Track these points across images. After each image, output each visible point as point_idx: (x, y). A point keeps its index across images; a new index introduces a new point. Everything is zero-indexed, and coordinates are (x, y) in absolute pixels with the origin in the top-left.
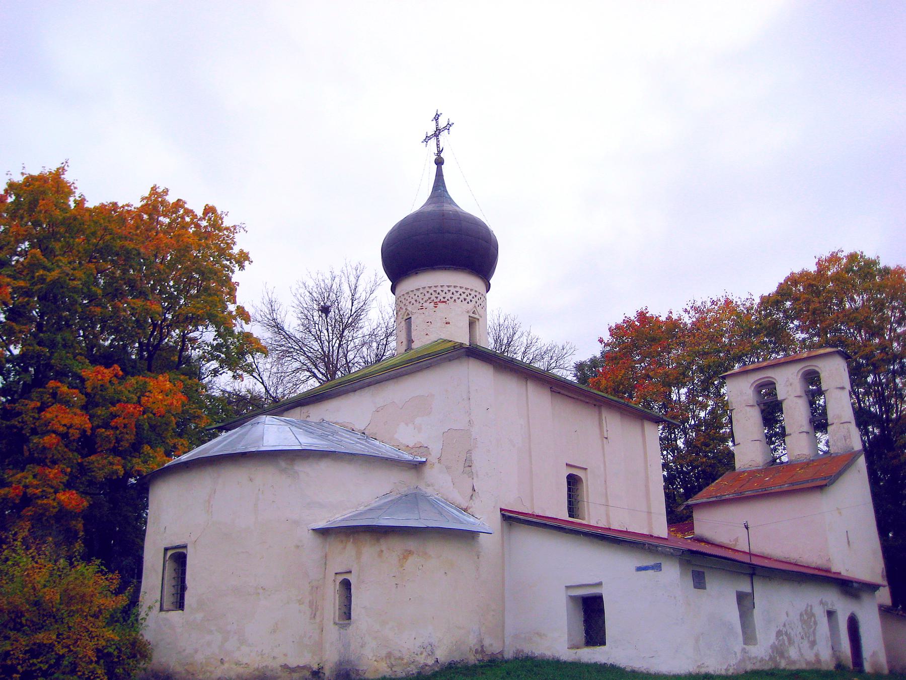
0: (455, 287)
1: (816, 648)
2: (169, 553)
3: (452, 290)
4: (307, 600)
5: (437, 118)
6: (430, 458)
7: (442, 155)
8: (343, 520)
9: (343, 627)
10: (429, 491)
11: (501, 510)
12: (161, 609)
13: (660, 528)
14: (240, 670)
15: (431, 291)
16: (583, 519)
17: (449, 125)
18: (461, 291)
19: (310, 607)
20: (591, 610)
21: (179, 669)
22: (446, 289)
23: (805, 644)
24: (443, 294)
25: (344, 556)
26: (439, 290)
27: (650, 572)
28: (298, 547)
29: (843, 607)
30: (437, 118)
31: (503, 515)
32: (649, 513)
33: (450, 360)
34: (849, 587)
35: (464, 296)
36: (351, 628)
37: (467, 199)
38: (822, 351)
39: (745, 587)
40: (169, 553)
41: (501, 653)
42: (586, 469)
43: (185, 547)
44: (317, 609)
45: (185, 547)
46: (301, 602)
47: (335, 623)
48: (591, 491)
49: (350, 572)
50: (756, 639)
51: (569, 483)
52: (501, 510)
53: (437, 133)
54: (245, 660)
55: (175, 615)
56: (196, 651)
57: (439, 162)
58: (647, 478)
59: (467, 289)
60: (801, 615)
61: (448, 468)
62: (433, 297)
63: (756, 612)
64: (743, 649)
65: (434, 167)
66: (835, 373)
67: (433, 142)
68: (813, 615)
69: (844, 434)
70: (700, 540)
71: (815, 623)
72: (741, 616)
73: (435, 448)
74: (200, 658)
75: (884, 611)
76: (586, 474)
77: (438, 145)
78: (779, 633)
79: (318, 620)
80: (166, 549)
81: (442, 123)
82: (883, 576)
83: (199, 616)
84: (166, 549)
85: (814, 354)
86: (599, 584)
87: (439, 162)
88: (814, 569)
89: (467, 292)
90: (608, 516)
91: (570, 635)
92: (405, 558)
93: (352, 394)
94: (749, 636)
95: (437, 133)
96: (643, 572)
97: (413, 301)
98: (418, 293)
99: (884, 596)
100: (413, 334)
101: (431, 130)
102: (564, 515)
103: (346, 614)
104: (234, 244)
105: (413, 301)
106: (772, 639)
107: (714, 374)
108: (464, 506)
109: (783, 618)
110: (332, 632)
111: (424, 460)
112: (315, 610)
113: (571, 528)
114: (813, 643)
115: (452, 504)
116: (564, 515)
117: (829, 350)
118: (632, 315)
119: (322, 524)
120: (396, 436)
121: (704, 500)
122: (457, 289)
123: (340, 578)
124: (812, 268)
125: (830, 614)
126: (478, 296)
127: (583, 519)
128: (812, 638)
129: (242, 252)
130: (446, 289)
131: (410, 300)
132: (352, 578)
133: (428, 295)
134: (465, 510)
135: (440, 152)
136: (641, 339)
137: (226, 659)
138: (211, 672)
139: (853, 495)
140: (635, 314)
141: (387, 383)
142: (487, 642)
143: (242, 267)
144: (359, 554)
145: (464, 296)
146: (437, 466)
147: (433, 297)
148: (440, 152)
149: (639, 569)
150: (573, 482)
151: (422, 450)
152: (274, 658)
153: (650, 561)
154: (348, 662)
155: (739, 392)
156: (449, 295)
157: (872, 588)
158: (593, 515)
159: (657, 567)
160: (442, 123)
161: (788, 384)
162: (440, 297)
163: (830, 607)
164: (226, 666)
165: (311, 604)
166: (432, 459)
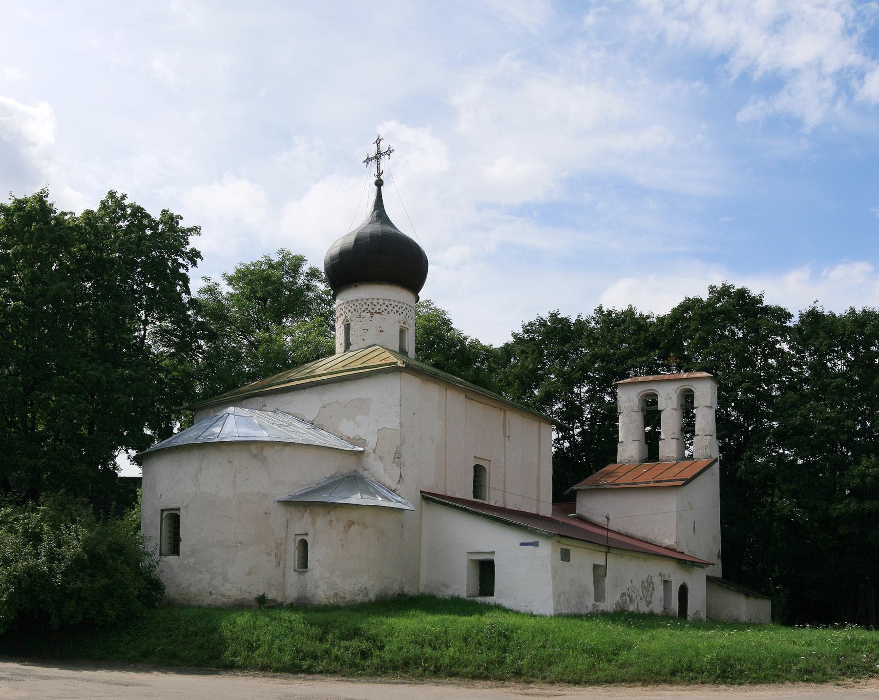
0: (389, 300)
1: (651, 606)
2: (165, 514)
3: (387, 303)
4: (273, 553)
6: (367, 449)
7: (382, 177)
8: (301, 495)
9: (300, 573)
10: (365, 474)
11: (421, 492)
12: (161, 554)
13: (547, 509)
14: (225, 600)
15: (368, 303)
16: (485, 500)
17: (390, 151)
18: (394, 304)
19: (276, 558)
20: (485, 570)
21: (177, 597)
22: (381, 302)
23: (643, 603)
24: (379, 306)
25: (302, 523)
26: (375, 303)
27: (530, 547)
28: (266, 513)
29: (678, 577)
30: (378, 142)
32: (538, 500)
34: (686, 563)
35: (397, 308)
36: (307, 575)
37: (404, 222)
38: (699, 374)
39: (600, 560)
40: (165, 514)
43: (179, 509)
44: (280, 560)
45: (179, 509)
46: (269, 554)
47: (295, 570)
48: (492, 480)
49: (307, 534)
50: (604, 598)
51: (475, 471)
52: (421, 492)
53: (378, 156)
54: (228, 593)
55: (172, 559)
56: (190, 585)
57: (379, 184)
58: (539, 469)
59: (399, 302)
60: (643, 582)
61: (381, 457)
62: (370, 308)
64: (594, 605)
65: (376, 187)
66: (705, 394)
67: (373, 163)
68: (653, 583)
69: (705, 444)
70: (581, 519)
71: (653, 589)
72: (595, 582)
73: (372, 441)
74: (193, 590)
75: (710, 580)
78: (623, 594)
79: (281, 567)
82: (718, 556)
83: (192, 561)
84: (162, 511)
85: (692, 376)
86: (493, 552)
87: (379, 184)
88: (667, 548)
89: (399, 305)
90: (504, 498)
91: (468, 587)
92: (349, 526)
93: (303, 391)
94: (599, 595)
95: (378, 156)
96: (525, 547)
97: (352, 310)
99: (717, 571)
100: (351, 338)
101: (373, 153)
102: (470, 497)
103: (304, 563)
104: (188, 244)
106: (617, 598)
107: (614, 373)
108: (393, 487)
109: (629, 584)
110: (293, 577)
111: (362, 449)
112: (279, 561)
113: (477, 506)
114: (649, 603)
115: (384, 486)
116: (470, 497)
117: (705, 374)
118: (545, 316)
119: (285, 497)
120: (339, 429)
121: (587, 487)
123: (299, 538)
124: (705, 296)
127: (485, 500)
128: (648, 599)
129: (193, 250)
130: (381, 302)
131: (349, 308)
132: (309, 539)
133: (365, 306)
134: (394, 491)
135: (379, 174)
136: (554, 337)
137: (214, 592)
138: (203, 601)
139: (707, 493)
140: (548, 315)
143: (194, 264)
144: (314, 522)
145: (397, 308)
146: (372, 455)
147: (370, 308)
148: (379, 174)
149: (522, 544)
151: (360, 442)
152: (250, 593)
153: (531, 539)
154: (306, 598)
155: (628, 400)
156: (384, 307)
157: (702, 565)
158: (493, 498)
159: (535, 544)
160: (384, 147)
161: (668, 399)
162: (376, 309)
163: (667, 578)
164: (214, 596)
165: (276, 556)
166: (369, 449)
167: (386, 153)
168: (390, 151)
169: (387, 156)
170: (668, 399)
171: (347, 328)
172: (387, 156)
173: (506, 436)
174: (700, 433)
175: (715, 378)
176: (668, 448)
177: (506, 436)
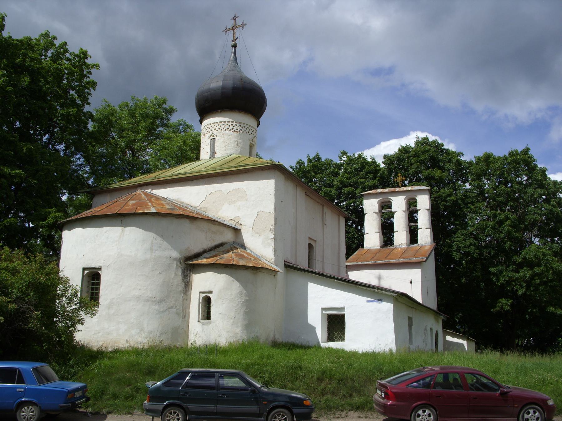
5: (235, 18)
7: (236, 42)
11: (285, 261)
17: (243, 25)
30: (235, 18)
31: (285, 264)
33: (262, 170)
35: (248, 130)
40: (86, 272)
41: (520, 355)
42: (316, 241)
45: (100, 269)
50: (482, 351)
52: (285, 261)
53: (234, 28)
59: (250, 126)
63: (413, 327)
66: (424, 202)
67: (230, 34)
69: (425, 235)
76: (315, 243)
77: (234, 35)
80: (84, 269)
81: (239, 22)
93: (190, 182)
95: (234, 28)
98: (221, 124)
105: (217, 129)
122: (245, 125)
125: (431, 329)
126: (253, 129)
131: (215, 127)
141: (217, 178)
142: (276, 337)
145: (248, 130)
150: (310, 246)
155: (371, 206)
158: (318, 268)
160: (239, 22)
161: (399, 204)
167: (229, 30)
168: (226, 30)
169: (241, 28)
170: (399, 204)
171: (213, 141)
172: (241, 28)
173: (324, 224)
174: (422, 227)
175: (431, 192)
176: (400, 237)
177: (324, 224)
